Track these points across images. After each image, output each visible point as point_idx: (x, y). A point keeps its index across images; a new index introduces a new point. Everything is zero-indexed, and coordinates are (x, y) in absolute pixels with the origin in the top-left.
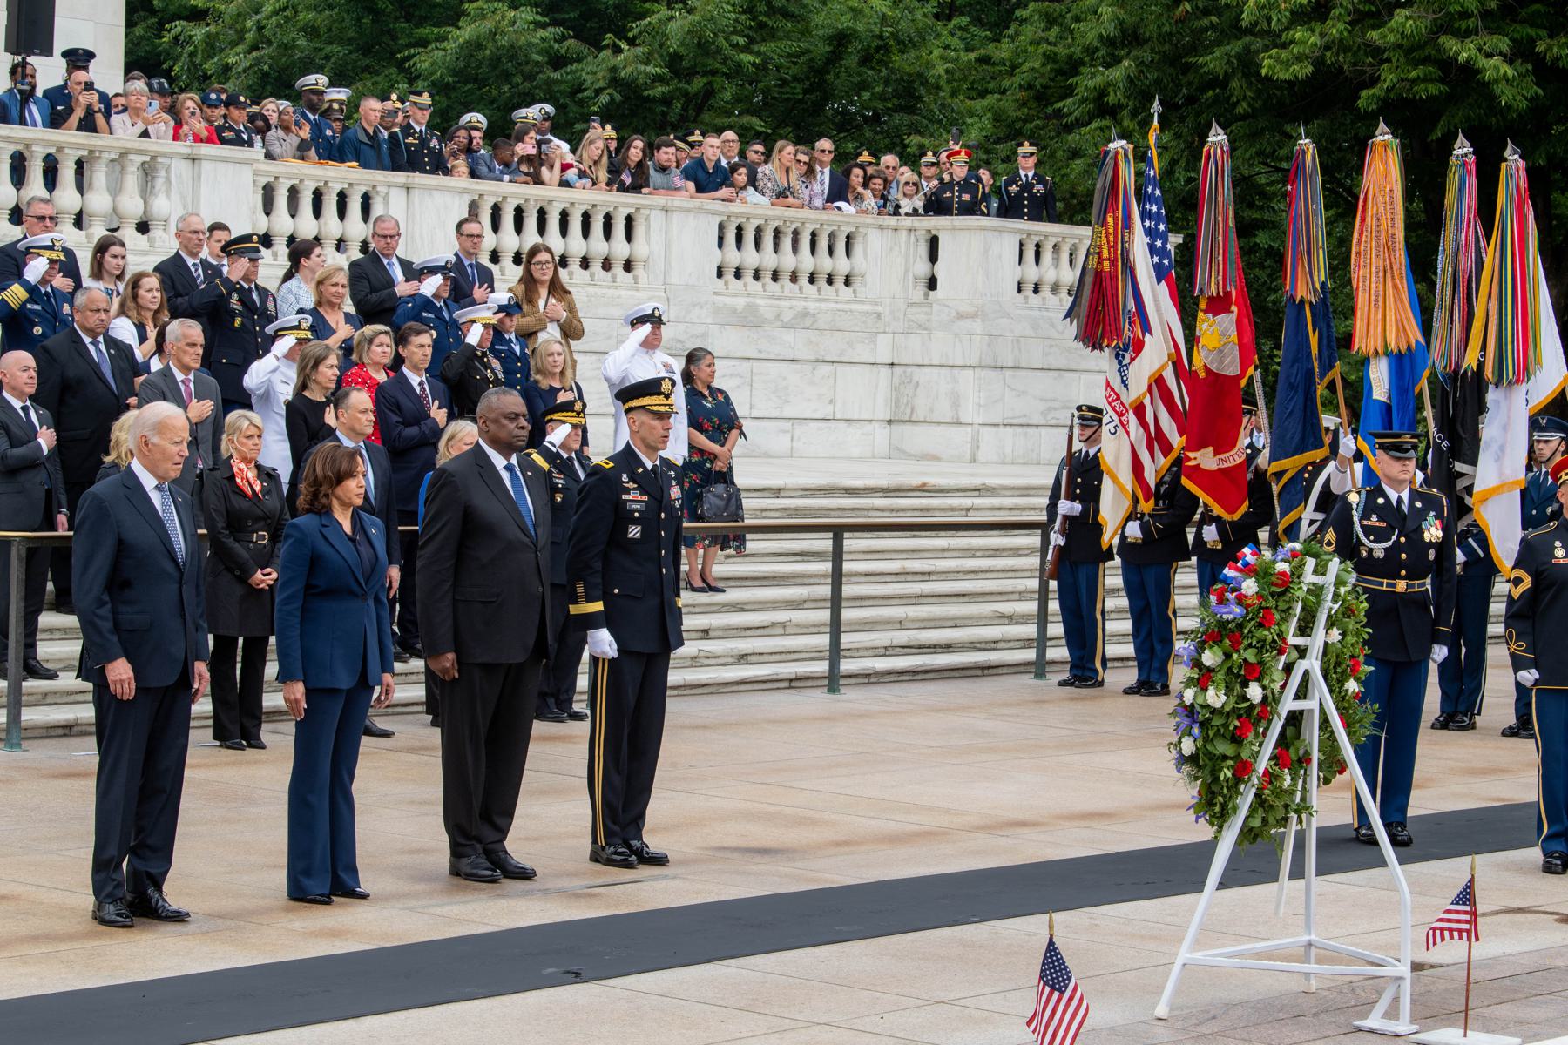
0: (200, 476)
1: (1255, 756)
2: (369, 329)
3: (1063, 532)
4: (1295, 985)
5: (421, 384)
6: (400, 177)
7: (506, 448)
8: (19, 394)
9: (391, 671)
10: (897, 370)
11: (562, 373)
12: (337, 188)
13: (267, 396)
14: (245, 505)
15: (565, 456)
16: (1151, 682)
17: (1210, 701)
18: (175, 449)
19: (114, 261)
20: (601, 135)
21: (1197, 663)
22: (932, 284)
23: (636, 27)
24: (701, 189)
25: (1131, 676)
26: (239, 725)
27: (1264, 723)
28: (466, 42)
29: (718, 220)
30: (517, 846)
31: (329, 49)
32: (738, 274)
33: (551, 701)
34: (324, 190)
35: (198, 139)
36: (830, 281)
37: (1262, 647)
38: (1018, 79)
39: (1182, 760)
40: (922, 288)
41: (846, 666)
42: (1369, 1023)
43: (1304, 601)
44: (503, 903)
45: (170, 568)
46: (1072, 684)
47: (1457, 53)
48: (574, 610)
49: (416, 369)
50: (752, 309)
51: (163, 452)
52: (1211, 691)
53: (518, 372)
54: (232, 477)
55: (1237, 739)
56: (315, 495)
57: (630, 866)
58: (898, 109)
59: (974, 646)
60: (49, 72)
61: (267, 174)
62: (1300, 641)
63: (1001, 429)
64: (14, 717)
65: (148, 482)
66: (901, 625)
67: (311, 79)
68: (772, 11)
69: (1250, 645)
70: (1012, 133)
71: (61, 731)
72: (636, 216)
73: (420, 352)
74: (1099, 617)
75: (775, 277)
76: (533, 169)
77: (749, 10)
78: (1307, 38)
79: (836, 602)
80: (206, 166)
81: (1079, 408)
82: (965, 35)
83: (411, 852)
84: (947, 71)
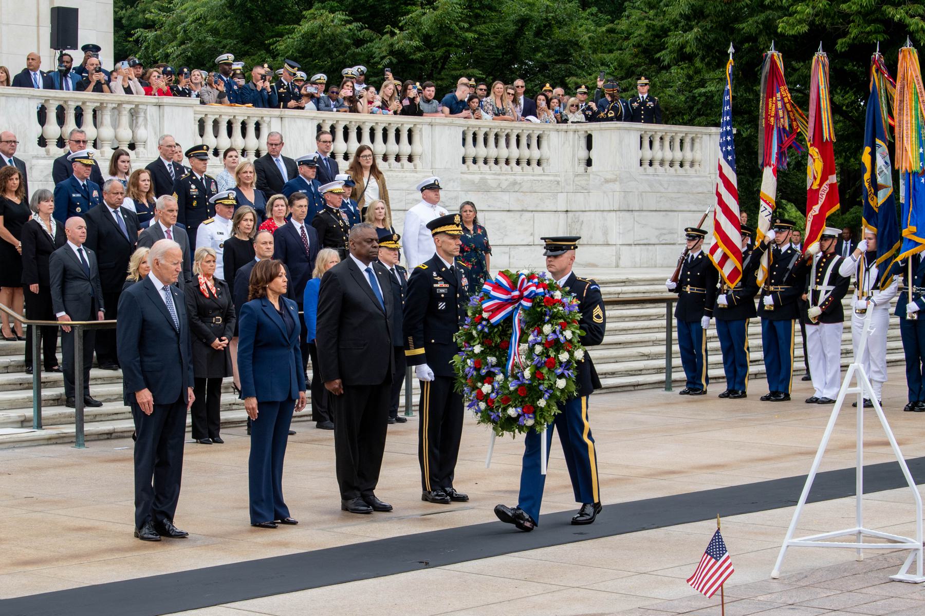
4: (850, 557)
5: (302, 228)
6: (276, 112)
8: (77, 243)
10: (570, 214)
11: (384, 220)
12: (241, 119)
14: (207, 302)
15: (389, 268)
18: (174, 267)
19: (123, 164)
20: (391, 83)
22: (589, 162)
23: (403, 20)
24: (452, 112)
25: (723, 387)
28: (306, 33)
29: (462, 129)
30: (381, 493)
31: (225, 42)
32: (475, 161)
34: (233, 121)
35: (161, 93)
36: (529, 163)
38: (633, 41)
40: (583, 165)
42: (898, 576)
44: (375, 525)
45: (172, 334)
46: (688, 393)
47: (893, 16)
48: (408, 353)
49: (298, 219)
50: (483, 181)
51: (167, 269)
54: (198, 286)
57: (446, 502)
58: (557, 62)
59: (629, 373)
60: (77, 57)
61: (200, 113)
63: (633, 247)
64: (80, 429)
65: (159, 285)
67: (224, 57)
68: (482, 7)
70: (630, 73)
71: (106, 436)
72: (413, 129)
73: (300, 210)
74: (704, 353)
75: (496, 162)
76: (353, 104)
77: (470, 7)
80: (167, 109)
81: (686, 230)
82: (596, 19)
83: (317, 498)
84: (590, 38)
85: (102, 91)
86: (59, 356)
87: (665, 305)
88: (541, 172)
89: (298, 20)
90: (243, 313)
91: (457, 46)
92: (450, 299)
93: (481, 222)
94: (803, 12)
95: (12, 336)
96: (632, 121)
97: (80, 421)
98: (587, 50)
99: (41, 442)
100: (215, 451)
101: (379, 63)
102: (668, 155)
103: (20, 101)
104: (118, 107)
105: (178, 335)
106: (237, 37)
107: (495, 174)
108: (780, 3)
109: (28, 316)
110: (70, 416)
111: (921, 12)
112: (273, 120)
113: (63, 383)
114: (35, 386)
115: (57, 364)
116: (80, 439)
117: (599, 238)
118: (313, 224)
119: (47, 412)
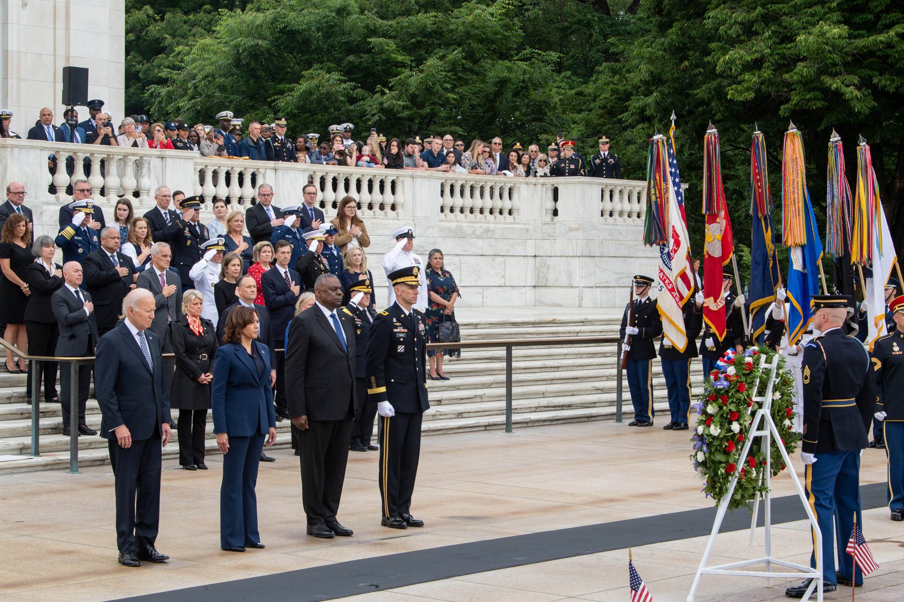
0: (170, 325)
1: (737, 461)
2: (259, 244)
3: (629, 343)
5: (285, 273)
6: (271, 164)
7: (331, 306)
8: (74, 285)
9: (274, 426)
10: (538, 259)
12: (238, 170)
13: (202, 282)
14: (194, 339)
15: (361, 309)
16: (679, 422)
17: (712, 432)
18: (147, 314)
20: (375, 140)
21: (704, 412)
22: (555, 213)
23: (393, 81)
24: (430, 166)
25: (667, 420)
26: (192, 457)
27: (741, 444)
28: (304, 91)
29: (441, 182)
30: (342, 518)
31: (232, 97)
33: (358, 440)
34: (231, 172)
35: (165, 146)
37: (739, 403)
38: (598, 103)
39: (698, 464)
40: (550, 215)
41: (515, 418)
43: (761, 378)
44: (336, 549)
45: (148, 376)
46: (636, 425)
48: (370, 392)
49: (282, 265)
51: (140, 316)
52: (712, 427)
53: (338, 266)
54: (188, 325)
55: (727, 452)
56: (233, 333)
57: (403, 528)
58: (533, 120)
61: (201, 164)
62: (759, 399)
63: (594, 289)
64: (74, 456)
65: (134, 331)
66: (543, 395)
67: (224, 113)
69: (732, 402)
71: (99, 463)
73: (283, 256)
74: (649, 388)
78: (751, 79)
79: (509, 384)
80: (169, 161)
81: (635, 277)
82: (569, 81)
83: (286, 523)
84: (560, 100)
85: (110, 144)
86: (58, 388)
87: (505, 348)
88: (512, 221)
89: (297, 79)
90: (217, 356)
91: (440, 105)
92: (407, 342)
93: (446, 268)
94: (750, 81)
95: (16, 369)
96: (593, 176)
97: (74, 448)
98: (559, 110)
99: (38, 468)
100: (199, 477)
101: (370, 120)
102: (627, 207)
103: (32, 152)
104: (124, 158)
105: (152, 376)
106: (243, 93)
107: (470, 222)
108: (729, 73)
109: (31, 352)
110: (66, 444)
111: (856, 82)
112: (268, 171)
113: (61, 413)
114: (33, 416)
115: (56, 395)
116: (74, 465)
117: (564, 281)
118: (298, 270)
119: (44, 440)
